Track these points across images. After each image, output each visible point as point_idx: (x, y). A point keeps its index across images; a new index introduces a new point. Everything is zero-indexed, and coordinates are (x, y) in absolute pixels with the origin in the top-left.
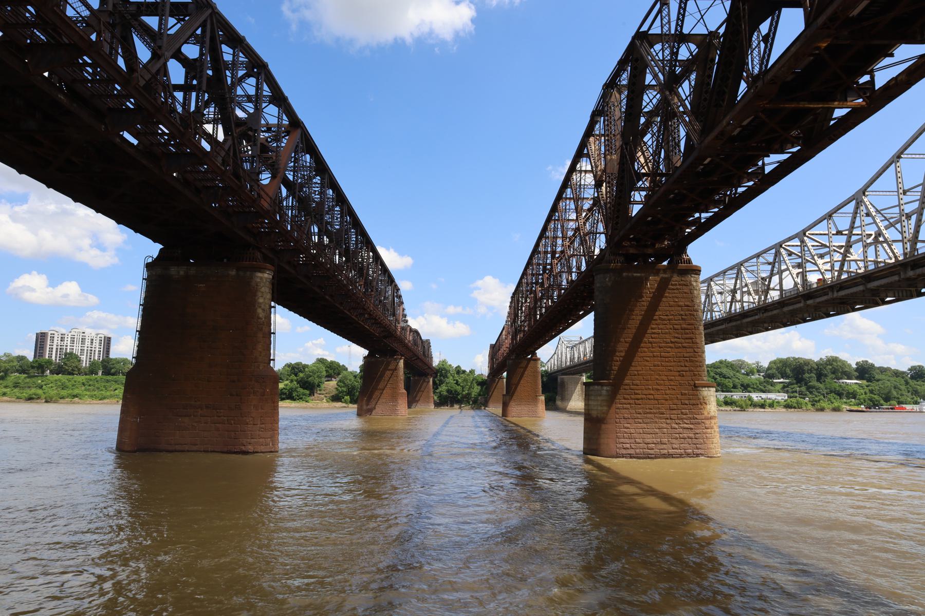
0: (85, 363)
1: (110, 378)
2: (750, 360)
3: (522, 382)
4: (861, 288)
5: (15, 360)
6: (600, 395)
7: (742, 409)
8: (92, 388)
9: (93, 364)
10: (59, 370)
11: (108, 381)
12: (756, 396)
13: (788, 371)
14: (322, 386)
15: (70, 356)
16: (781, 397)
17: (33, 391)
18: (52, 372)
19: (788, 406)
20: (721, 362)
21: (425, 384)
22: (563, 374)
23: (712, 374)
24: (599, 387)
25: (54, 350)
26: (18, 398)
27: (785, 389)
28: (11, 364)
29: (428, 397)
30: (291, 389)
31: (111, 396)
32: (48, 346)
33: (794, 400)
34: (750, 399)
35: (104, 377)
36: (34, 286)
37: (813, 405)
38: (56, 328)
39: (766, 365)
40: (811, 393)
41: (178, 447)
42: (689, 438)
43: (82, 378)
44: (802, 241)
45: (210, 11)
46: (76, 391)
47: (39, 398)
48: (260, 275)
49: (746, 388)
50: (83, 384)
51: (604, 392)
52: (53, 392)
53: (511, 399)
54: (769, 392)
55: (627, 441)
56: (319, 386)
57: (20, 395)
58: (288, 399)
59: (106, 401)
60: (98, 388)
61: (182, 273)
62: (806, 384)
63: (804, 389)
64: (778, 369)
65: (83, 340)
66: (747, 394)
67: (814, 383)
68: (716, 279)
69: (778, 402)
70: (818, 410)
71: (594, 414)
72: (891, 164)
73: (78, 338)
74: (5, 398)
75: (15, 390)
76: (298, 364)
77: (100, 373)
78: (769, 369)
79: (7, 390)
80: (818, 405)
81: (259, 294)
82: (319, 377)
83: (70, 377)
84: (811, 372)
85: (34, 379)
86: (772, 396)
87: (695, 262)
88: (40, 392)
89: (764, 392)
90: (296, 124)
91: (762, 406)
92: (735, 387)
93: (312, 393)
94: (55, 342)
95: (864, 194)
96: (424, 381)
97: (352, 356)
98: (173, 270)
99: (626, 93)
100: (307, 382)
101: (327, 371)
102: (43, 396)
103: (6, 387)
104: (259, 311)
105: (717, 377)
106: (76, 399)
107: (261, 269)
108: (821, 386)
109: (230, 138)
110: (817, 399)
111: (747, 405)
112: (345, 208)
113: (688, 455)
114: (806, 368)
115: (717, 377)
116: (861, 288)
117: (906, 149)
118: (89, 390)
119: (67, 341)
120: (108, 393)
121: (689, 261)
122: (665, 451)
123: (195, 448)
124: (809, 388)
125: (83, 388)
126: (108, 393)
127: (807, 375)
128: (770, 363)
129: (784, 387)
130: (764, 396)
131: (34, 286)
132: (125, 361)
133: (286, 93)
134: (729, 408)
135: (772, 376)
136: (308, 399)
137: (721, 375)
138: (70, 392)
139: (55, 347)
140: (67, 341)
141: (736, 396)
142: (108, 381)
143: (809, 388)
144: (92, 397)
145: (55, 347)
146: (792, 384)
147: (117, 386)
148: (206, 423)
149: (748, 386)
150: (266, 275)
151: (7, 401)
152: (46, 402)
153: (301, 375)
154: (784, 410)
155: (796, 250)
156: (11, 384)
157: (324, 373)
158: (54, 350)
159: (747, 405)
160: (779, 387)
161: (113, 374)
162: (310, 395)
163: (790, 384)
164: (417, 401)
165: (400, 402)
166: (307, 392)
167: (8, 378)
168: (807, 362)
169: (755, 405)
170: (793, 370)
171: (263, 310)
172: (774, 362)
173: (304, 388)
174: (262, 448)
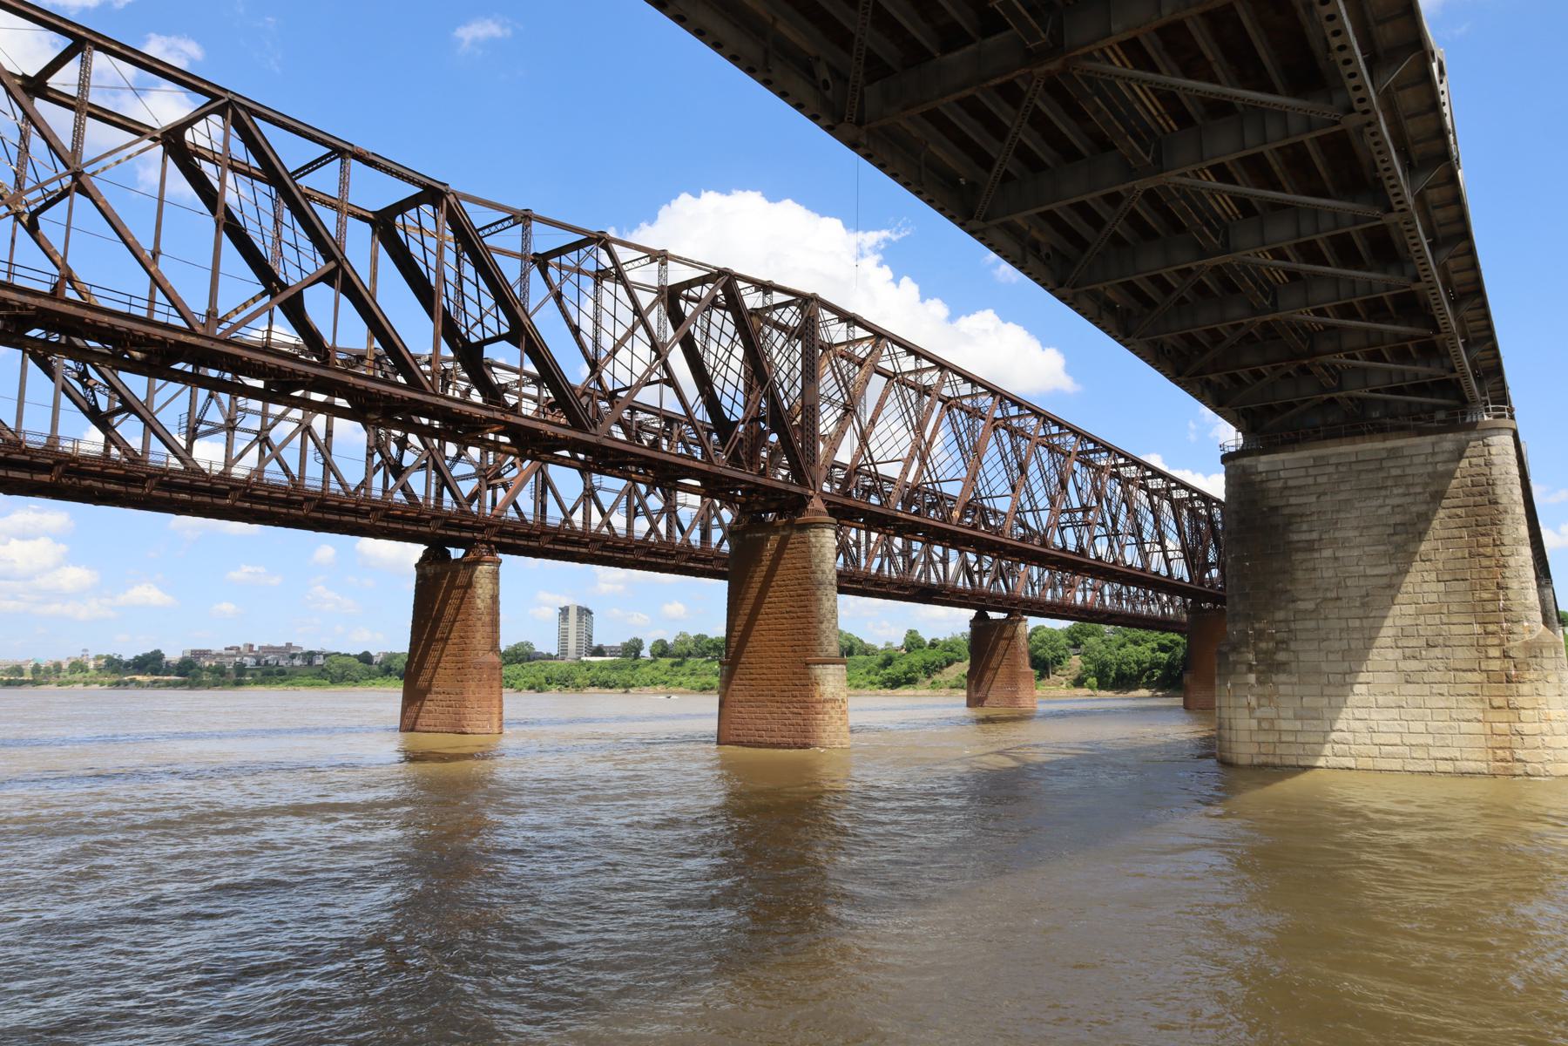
151: (168, 684)
156: (688, 672)
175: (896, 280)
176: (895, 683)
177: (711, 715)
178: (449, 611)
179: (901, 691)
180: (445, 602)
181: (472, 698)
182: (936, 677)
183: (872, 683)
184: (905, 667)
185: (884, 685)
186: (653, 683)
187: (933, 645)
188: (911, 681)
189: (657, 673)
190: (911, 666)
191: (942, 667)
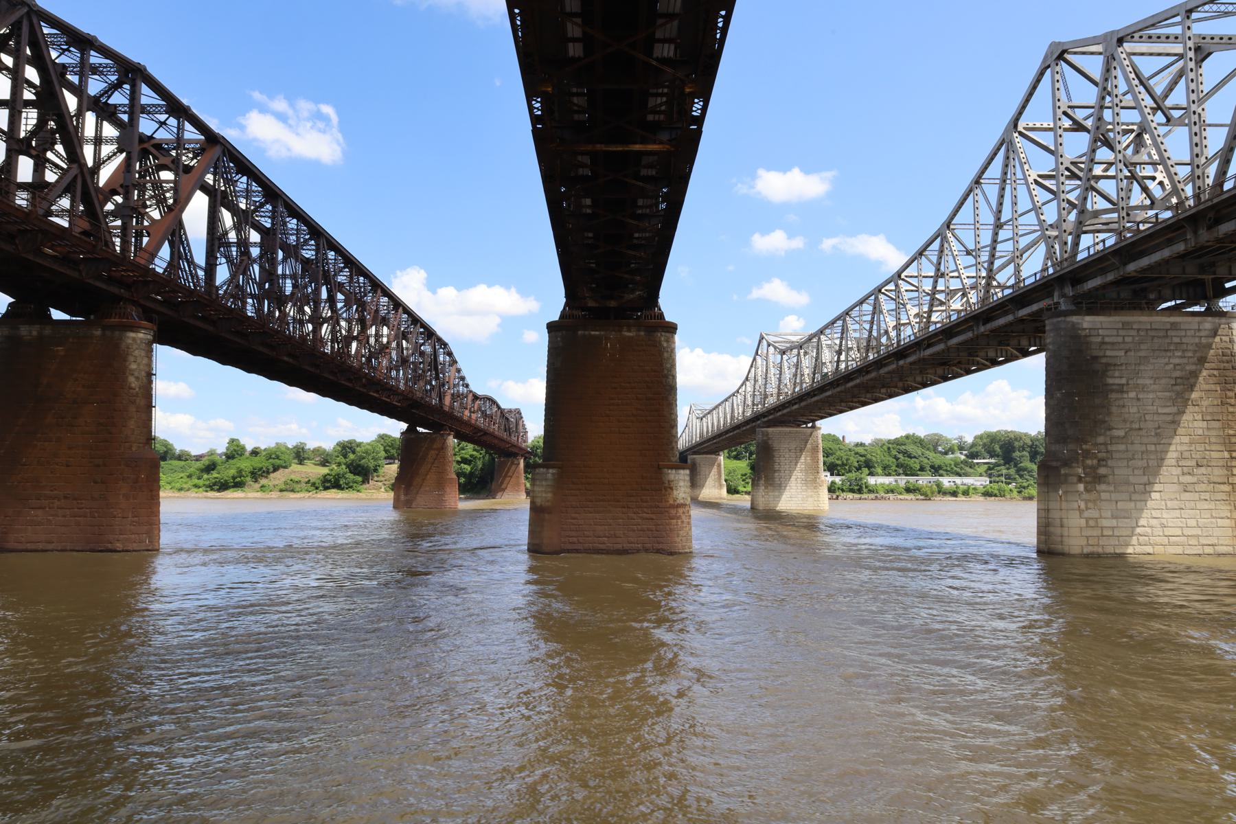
2: (951, 433)
4: (941, 347)
7: (927, 497)
12: (946, 482)
14: (381, 471)
16: (981, 482)
19: (987, 494)
20: (907, 437)
21: (513, 467)
22: (695, 453)
23: (894, 452)
29: (518, 484)
33: (995, 486)
34: (939, 485)
37: (1020, 492)
39: (969, 439)
40: (1021, 476)
41: (29, 546)
42: (649, 530)
44: (897, 286)
45: (25, 10)
48: (132, 335)
49: (936, 470)
51: (549, 476)
54: (966, 475)
55: (573, 534)
56: (376, 470)
58: (334, 487)
61: (35, 333)
62: (1016, 466)
63: (1012, 471)
64: (984, 445)
68: (828, 331)
69: (975, 489)
70: (1025, 499)
71: (539, 501)
72: (968, 195)
76: (350, 442)
78: (973, 445)
80: (1026, 493)
81: (131, 359)
82: (375, 459)
84: (1024, 450)
86: (969, 481)
87: (668, 318)
89: (959, 475)
90: (212, 139)
91: (954, 494)
92: (922, 469)
93: (366, 480)
95: (948, 227)
96: (513, 463)
97: (372, 428)
98: (24, 330)
100: (359, 466)
101: (386, 451)
104: (132, 379)
105: (900, 456)
107: (134, 328)
109: (75, 166)
111: (933, 493)
112: (323, 241)
113: (647, 551)
114: (1016, 444)
115: (900, 456)
116: (941, 347)
117: (983, 172)
121: (661, 316)
122: (619, 546)
123: (50, 547)
124: (1020, 471)
127: (1017, 454)
129: (989, 469)
130: (958, 480)
133: (185, 101)
134: (910, 496)
135: (973, 455)
137: (905, 453)
141: (923, 481)
143: (1020, 471)
146: (999, 465)
148: (64, 516)
149: (940, 467)
150: (141, 335)
153: (352, 456)
154: (982, 498)
155: (893, 295)
157: (383, 454)
159: (933, 493)
160: (983, 469)
162: (363, 482)
163: (997, 465)
164: (504, 490)
165: (448, 490)
166: (360, 479)
168: (1018, 437)
169: (942, 492)
171: (137, 378)
172: (981, 437)
174: (135, 546)
176: (223, 486)
179: (230, 494)
182: (263, 481)
183: (196, 486)
184: (233, 472)
185: (211, 487)
187: (255, 453)
188: (238, 485)
190: (240, 471)
191: (268, 473)
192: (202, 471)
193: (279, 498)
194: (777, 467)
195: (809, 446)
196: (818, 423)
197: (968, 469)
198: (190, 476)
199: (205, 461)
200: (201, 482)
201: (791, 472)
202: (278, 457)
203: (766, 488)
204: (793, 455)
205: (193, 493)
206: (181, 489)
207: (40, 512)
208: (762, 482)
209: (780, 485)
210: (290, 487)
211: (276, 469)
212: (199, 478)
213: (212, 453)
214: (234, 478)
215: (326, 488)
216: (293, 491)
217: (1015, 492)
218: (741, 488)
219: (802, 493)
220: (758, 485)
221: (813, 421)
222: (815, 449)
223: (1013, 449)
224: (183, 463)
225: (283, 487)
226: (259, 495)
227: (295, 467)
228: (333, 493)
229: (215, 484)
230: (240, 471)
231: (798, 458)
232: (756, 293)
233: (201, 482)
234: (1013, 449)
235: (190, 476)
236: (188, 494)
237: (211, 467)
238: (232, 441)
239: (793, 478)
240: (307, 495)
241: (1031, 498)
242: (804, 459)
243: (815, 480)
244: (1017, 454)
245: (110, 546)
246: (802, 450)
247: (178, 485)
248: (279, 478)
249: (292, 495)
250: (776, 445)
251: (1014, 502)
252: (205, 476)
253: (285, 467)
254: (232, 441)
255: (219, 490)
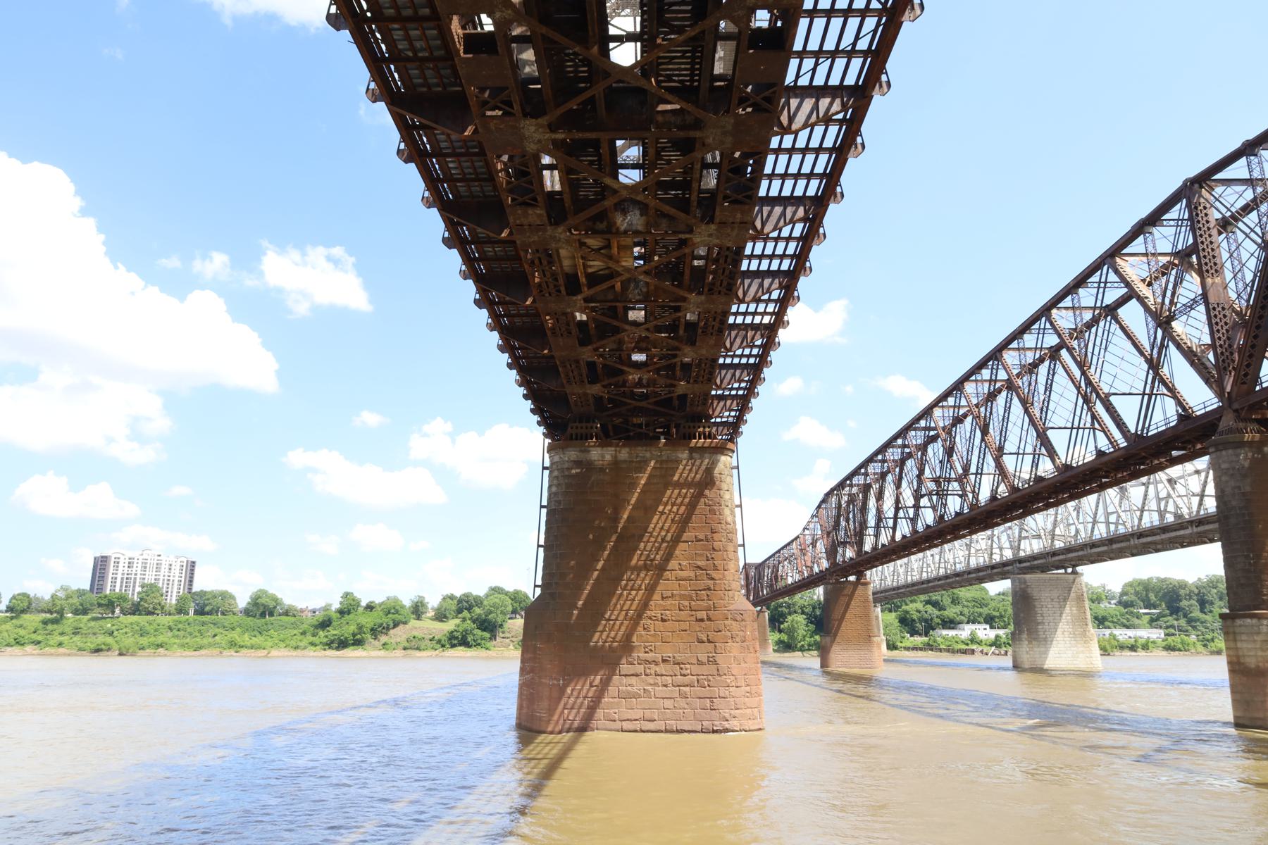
0: (172, 600)
1: (206, 618)
3: (848, 616)
5: (75, 597)
6: (1259, 633)
8: (181, 633)
9: (181, 600)
10: (136, 609)
11: (204, 624)
13: (1152, 597)
14: (506, 626)
15: (150, 589)
16: (1156, 634)
17: (101, 639)
18: (123, 612)
19: (1169, 648)
24: (1255, 621)
25: (119, 581)
26: (80, 649)
27: (1153, 622)
28: (70, 601)
30: (466, 631)
31: (210, 645)
32: (110, 576)
34: (1114, 638)
35: (199, 617)
36: (46, 495)
37: (1205, 646)
38: (119, 547)
40: (1194, 628)
43: (165, 620)
46: (161, 639)
47: (109, 650)
50: (170, 629)
52: (129, 641)
53: (832, 642)
56: (501, 626)
57: (82, 645)
58: (460, 645)
59: (203, 652)
60: (191, 634)
62: (1185, 616)
63: (1183, 622)
65: (158, 566)
66: (1107, 632)
67: (1196, 613)
69: (1154, 642)
70: (1213, 653)
71: (1251, 662)
73: (152, 563)
74: (61, 650)
75: (76, 638)
76: (467, 595)
77: (191, 612)
78: (1123, 594)
79: (64, 639)
80: (1213, 646)
83: (150, 618)
84: (1191, 598)
85: (101, 623)
88: (109, 640)
89: (1128, 627)
91: (1133, 648)
93: (493, 637)
94: (121, 568)
99: (164, 261)
102: (115, 647)
103: (62, 634)
106: (161, 650)
108: (1208, 618)
110: (1209, 637)
114: (1182, 592)
118: (177, 636)
119: (137, 568)
120: (205, 641)
125: (170, 634)
126: (205, 641)
127: (1184, 603)
128: (1125, 585)
130: (1131, 633)
131: (46, 495)
132: (1212, 583)
133: (1178, 184)
136: (488, 645)
138: (152, 639)
139: (119, 577)
140: (137, 568)
142: (204, 624)
144: (183, 646)
145: (119, 577)
147: (217, 630)
151: (65, 655)
152: (120, 654)
154: (1165, 653)
156: (68, 630)
158: (119, 581)
161: (209, 613)
163: (1160, 616)
166: (487, 635)
167: (65, 621)
168: (1183, 585)
170: (1162, 598)
172: (1130, 584)
173: (484, 630)
175: (304, 254)
176: (342, 644)
177: (1217, 686)
178: (660, 525)
179: (349, 652)
180: (647, 508)
181: (735, 669)
182: (383, 639)
183: (313, 644)
184: (353, 628)
185: (329, 645)
186: (19, 642)
187: (370, 607)
188: (358, 643)
189: (22, 632)
190: (360, 628)
191: (388, 629)
192: (316, 627)
193: (404, 656)
194: (1039, 618)
195: (1073, 595)
196: (1079, 569)
197: (1136, 621)
198: (304, 633)
199: (320, 616)
200: (316, 640)
201: (1056, 624)
202: (397, 612)
203: (1030, 642)
204: (1057, 605)
205: (311, 652)
206: (296, 648)
207: (633, 680)
208: (1025, 636)
209: (1045, 640)
210: (413, 645)
211: (396, 625)
212: (314, 635)
213: (326, 608)
214: (354, 635)
215: (453, 646)
216: (418, 649)
217: (1199, 645)
218: (899, 644)
219: (1069, 648)
220: (1020, 640)
221: (1074, 566)
222: (1080, 598)
223: (1179, 598)
224: (293, 619)
225: (407, 645)
226: (382, 653)
227: (413, 623)
228: (460, 651)
229: (332, 642)
230: (360, 628)
231: (1062, 608)
232: (297, 458)
233: (316, 640)
234: (1179, 598)
235: (304, 633)
236: (305, 652)
237: (325, 624)
238: (346, 595)
239: (1059, 631)
240: (434, 653)
241: (1219, 652)
242: (1069, 609)
243: (1084, 634)
244: (1184, 603)
245: (727, 725)
246: (1065, 600)
247: (293, 643)
248: (399, 634)
249: (417, 653)
250: (1035, 594)
251: (1200, 658)
252: (321, 633)
253: (405, 623)
254: (346, 595)
255: (337, 649)
